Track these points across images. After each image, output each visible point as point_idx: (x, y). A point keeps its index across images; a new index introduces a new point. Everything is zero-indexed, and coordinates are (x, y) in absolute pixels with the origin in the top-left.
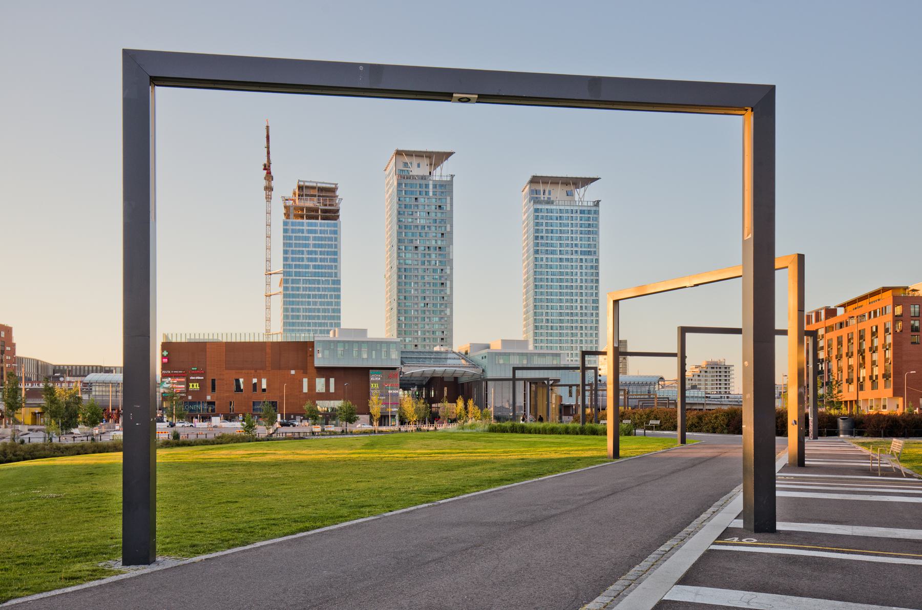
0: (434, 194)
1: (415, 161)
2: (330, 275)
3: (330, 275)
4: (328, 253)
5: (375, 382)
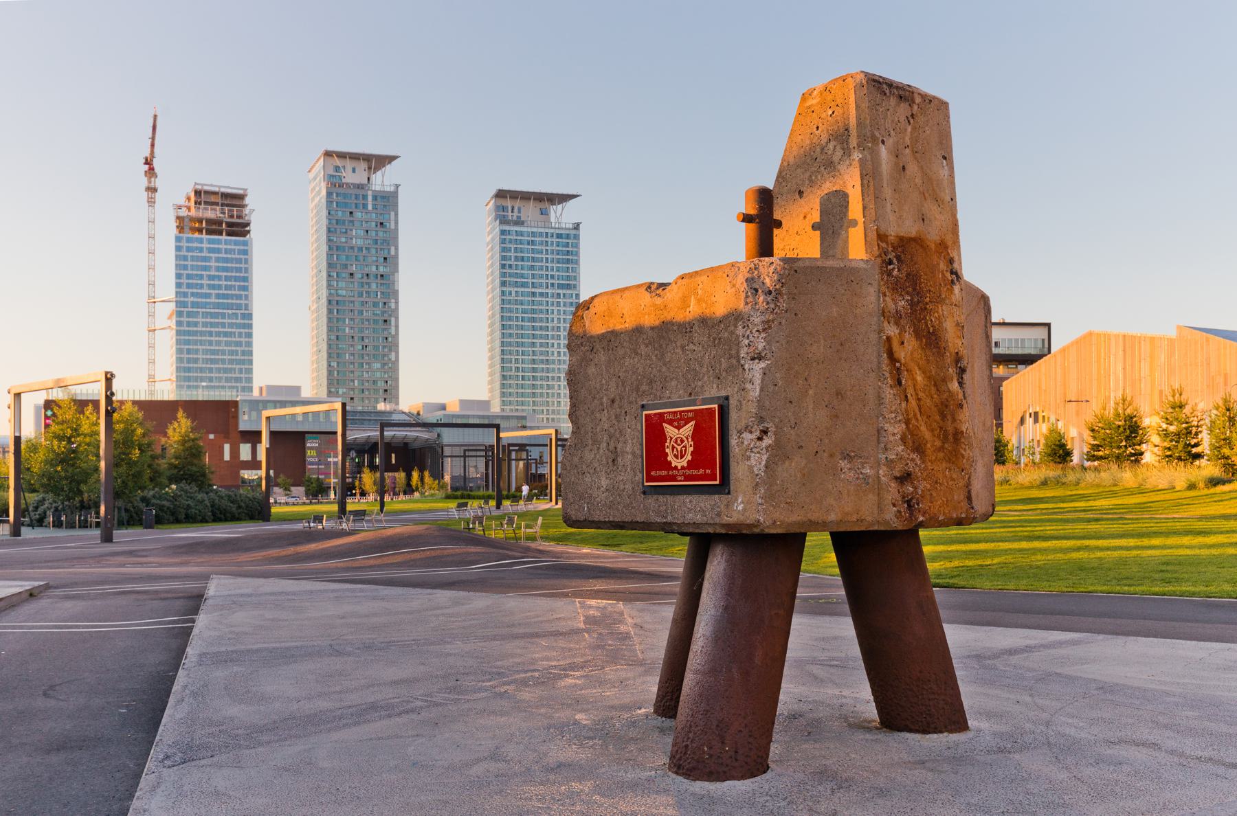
2: (239, 307)
3: (239, 307)
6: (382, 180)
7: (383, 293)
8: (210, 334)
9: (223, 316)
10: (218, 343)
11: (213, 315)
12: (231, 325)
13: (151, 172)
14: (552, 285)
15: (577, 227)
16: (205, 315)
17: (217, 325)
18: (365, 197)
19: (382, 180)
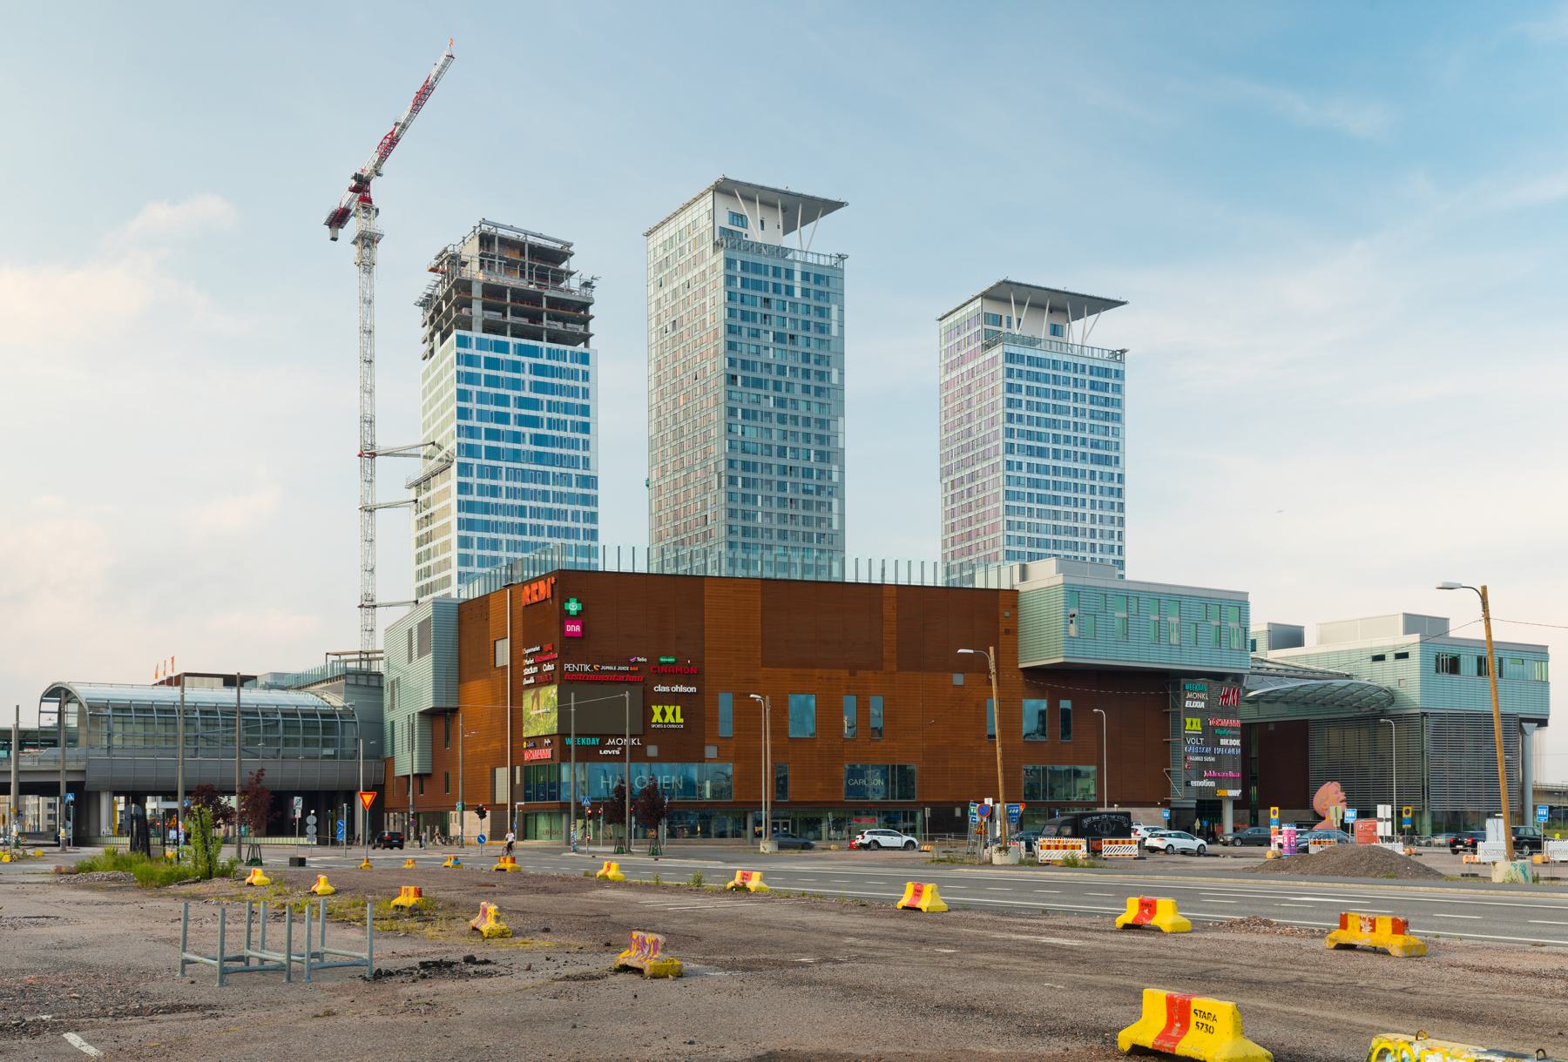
0: (805, 293)
1: (754, 215)
2: (573, 462)
3: (573, 462)
4: (567, 408)
5: (1194, 712)
6: (811, 243)
7: (817, 453)
8: (521, 511)
9: (544, 478)
10: (537, 530)
11: (524, 476)
12: (559, 497)
13: (392, 142)
14: (1084, 455)
15: (354, 243)
16: (514, 474)
17: (534, 495)
18: (789, 274)
19: (811, 243)
